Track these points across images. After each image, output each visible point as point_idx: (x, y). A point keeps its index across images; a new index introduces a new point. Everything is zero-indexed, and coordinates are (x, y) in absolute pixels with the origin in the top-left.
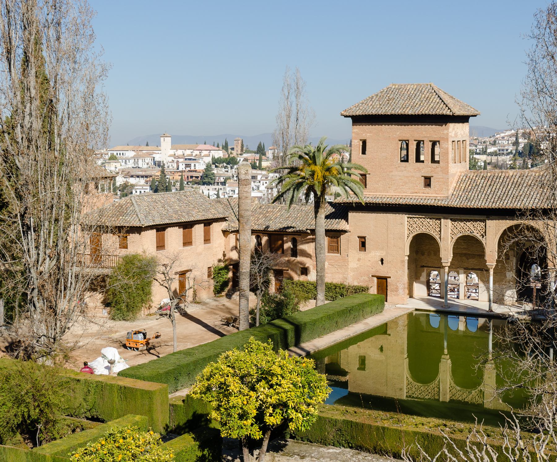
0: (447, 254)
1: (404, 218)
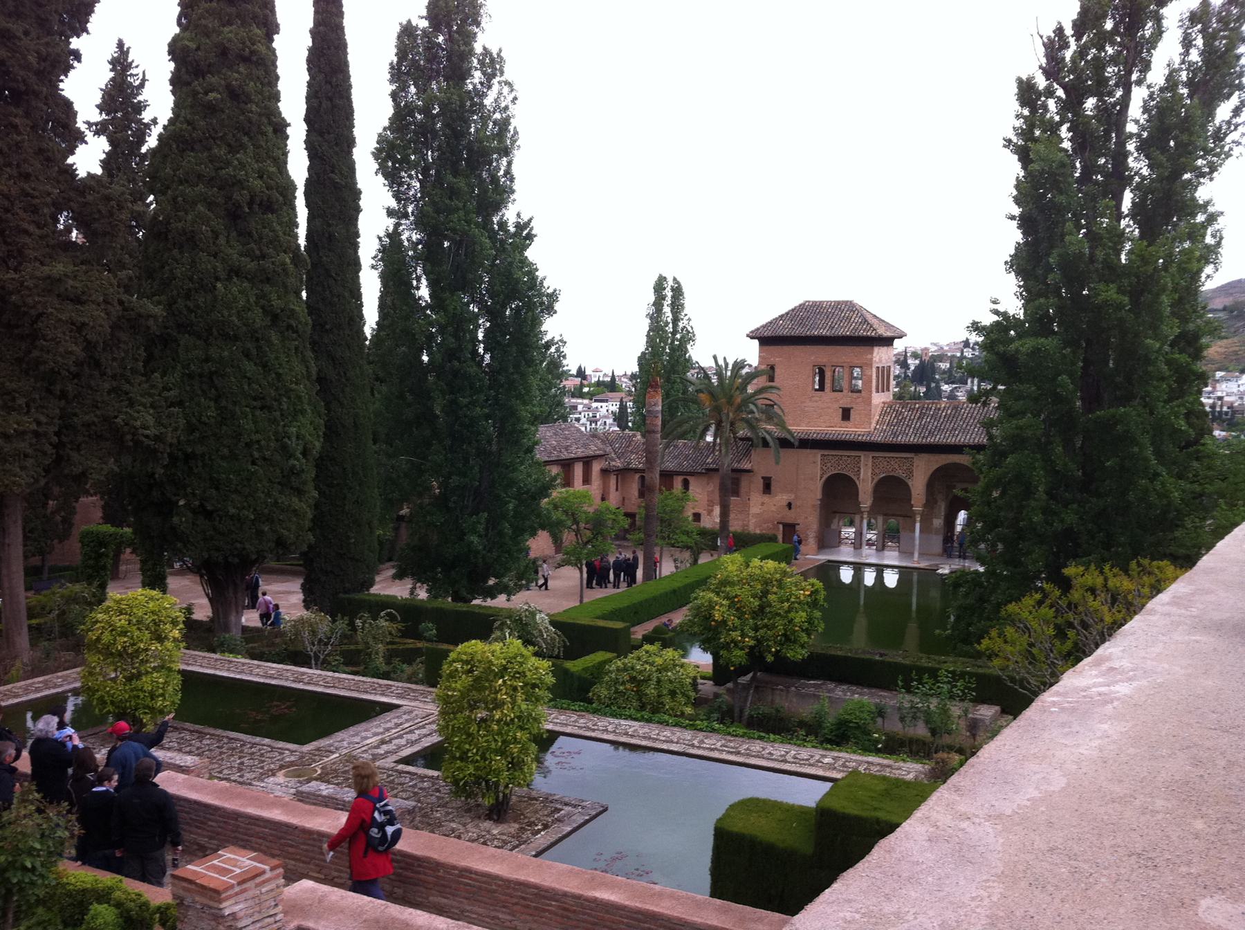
0: (866, 498)
1: (817, 455)
